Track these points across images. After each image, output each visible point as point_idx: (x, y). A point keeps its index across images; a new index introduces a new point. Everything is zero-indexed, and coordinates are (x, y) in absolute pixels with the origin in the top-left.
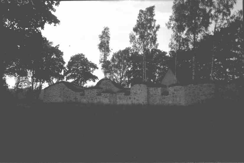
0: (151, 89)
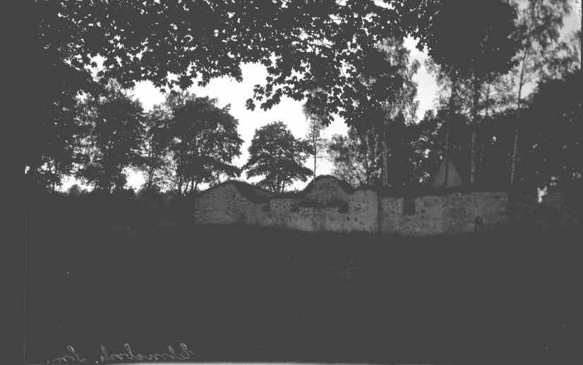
0: (385, 201)
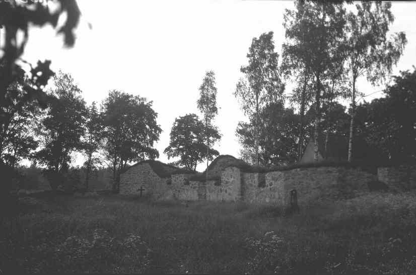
0: (247, 175)
